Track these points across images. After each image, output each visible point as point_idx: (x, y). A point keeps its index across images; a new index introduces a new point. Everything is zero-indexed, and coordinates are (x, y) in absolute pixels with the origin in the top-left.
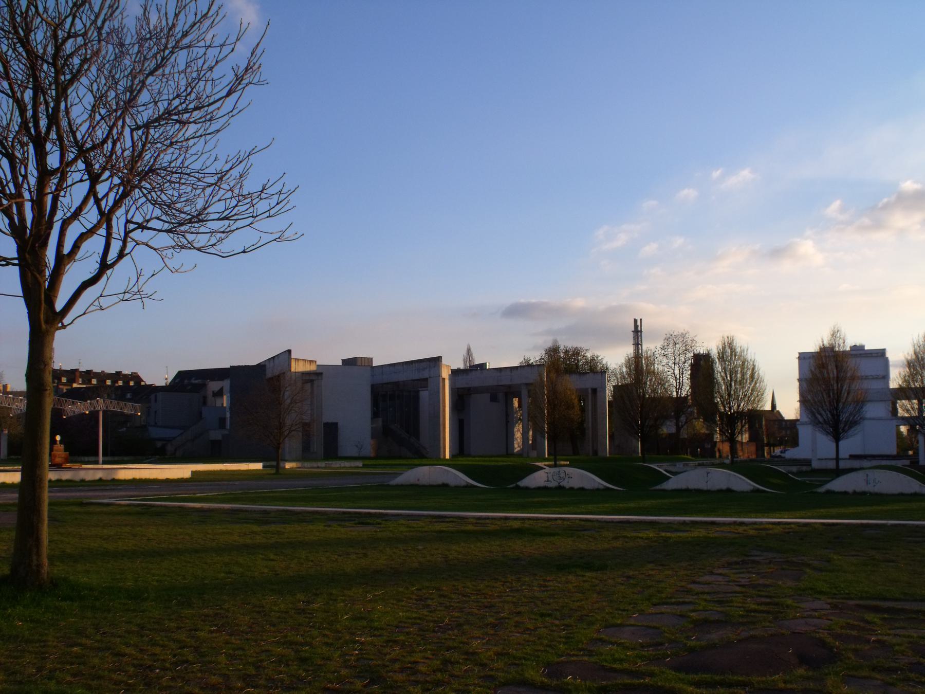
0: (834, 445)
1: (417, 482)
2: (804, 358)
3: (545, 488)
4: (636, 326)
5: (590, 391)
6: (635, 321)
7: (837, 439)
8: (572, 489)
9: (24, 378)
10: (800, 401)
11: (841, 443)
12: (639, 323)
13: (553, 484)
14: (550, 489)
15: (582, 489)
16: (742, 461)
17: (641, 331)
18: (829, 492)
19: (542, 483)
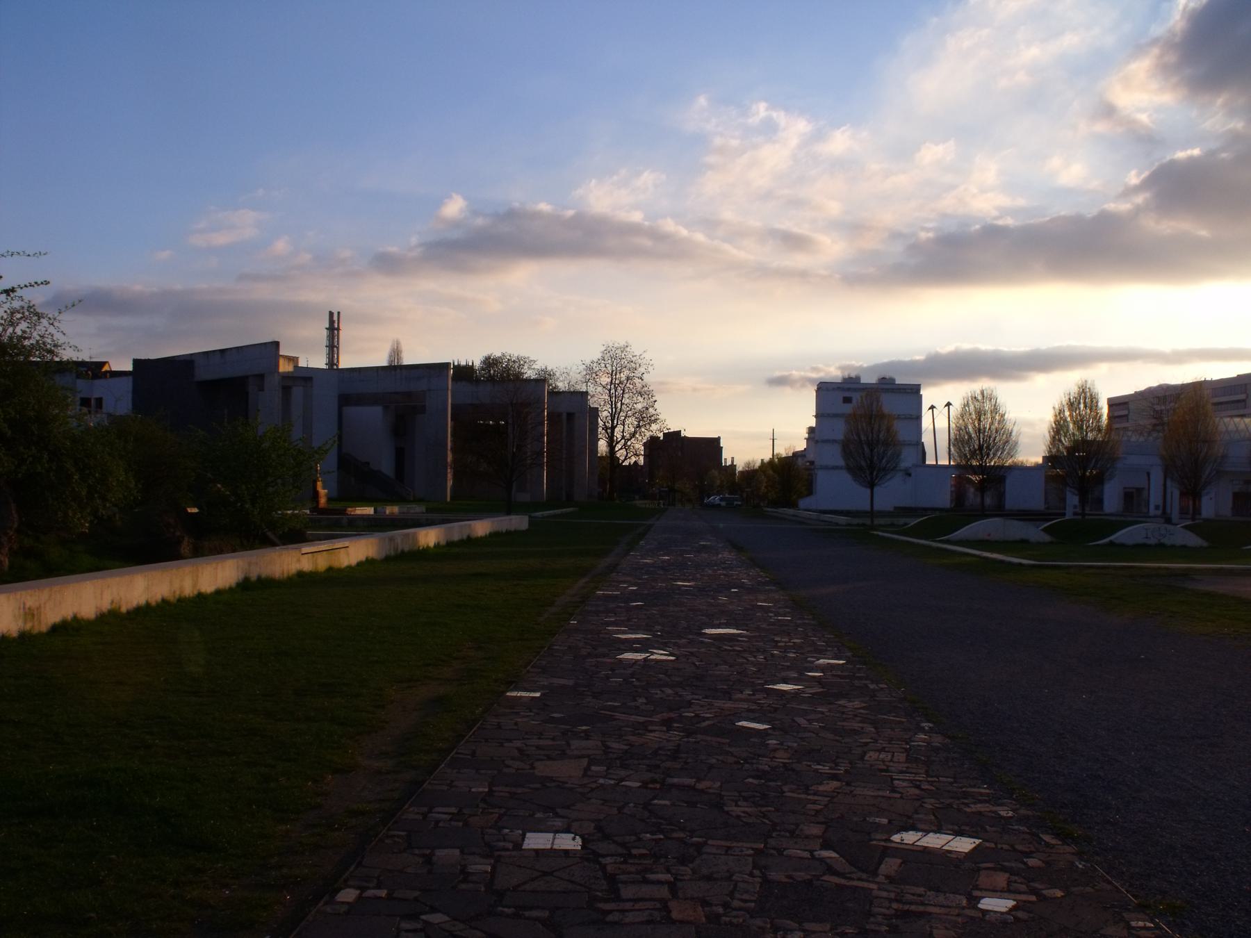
0: (868, 491)
1: (987, 538)
2: (827, 390)
3: (1145, 545)
4: (332, 322)
5: (564, 417)
6: (331, 314)
7: (871, 486)
8: (1173, 546)
9: (1154, 384)
10: (808, 440)
11: (875, 489)
12: (335, 318)
13: (1152, 541)
14: (1150, 546)
15: (1184, 547)
16: (1206, 520)
17: (338, 329)
18: (1112, 543)
19: (1140, 539)
